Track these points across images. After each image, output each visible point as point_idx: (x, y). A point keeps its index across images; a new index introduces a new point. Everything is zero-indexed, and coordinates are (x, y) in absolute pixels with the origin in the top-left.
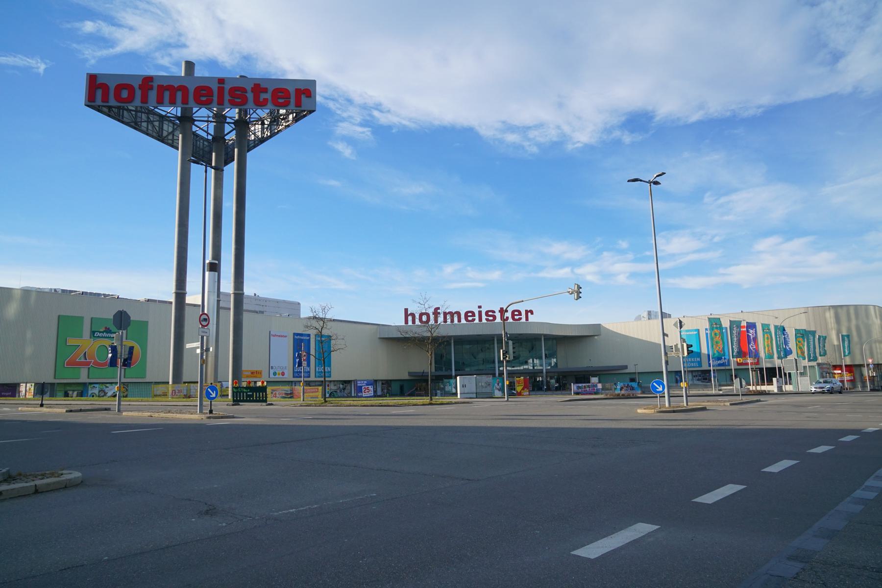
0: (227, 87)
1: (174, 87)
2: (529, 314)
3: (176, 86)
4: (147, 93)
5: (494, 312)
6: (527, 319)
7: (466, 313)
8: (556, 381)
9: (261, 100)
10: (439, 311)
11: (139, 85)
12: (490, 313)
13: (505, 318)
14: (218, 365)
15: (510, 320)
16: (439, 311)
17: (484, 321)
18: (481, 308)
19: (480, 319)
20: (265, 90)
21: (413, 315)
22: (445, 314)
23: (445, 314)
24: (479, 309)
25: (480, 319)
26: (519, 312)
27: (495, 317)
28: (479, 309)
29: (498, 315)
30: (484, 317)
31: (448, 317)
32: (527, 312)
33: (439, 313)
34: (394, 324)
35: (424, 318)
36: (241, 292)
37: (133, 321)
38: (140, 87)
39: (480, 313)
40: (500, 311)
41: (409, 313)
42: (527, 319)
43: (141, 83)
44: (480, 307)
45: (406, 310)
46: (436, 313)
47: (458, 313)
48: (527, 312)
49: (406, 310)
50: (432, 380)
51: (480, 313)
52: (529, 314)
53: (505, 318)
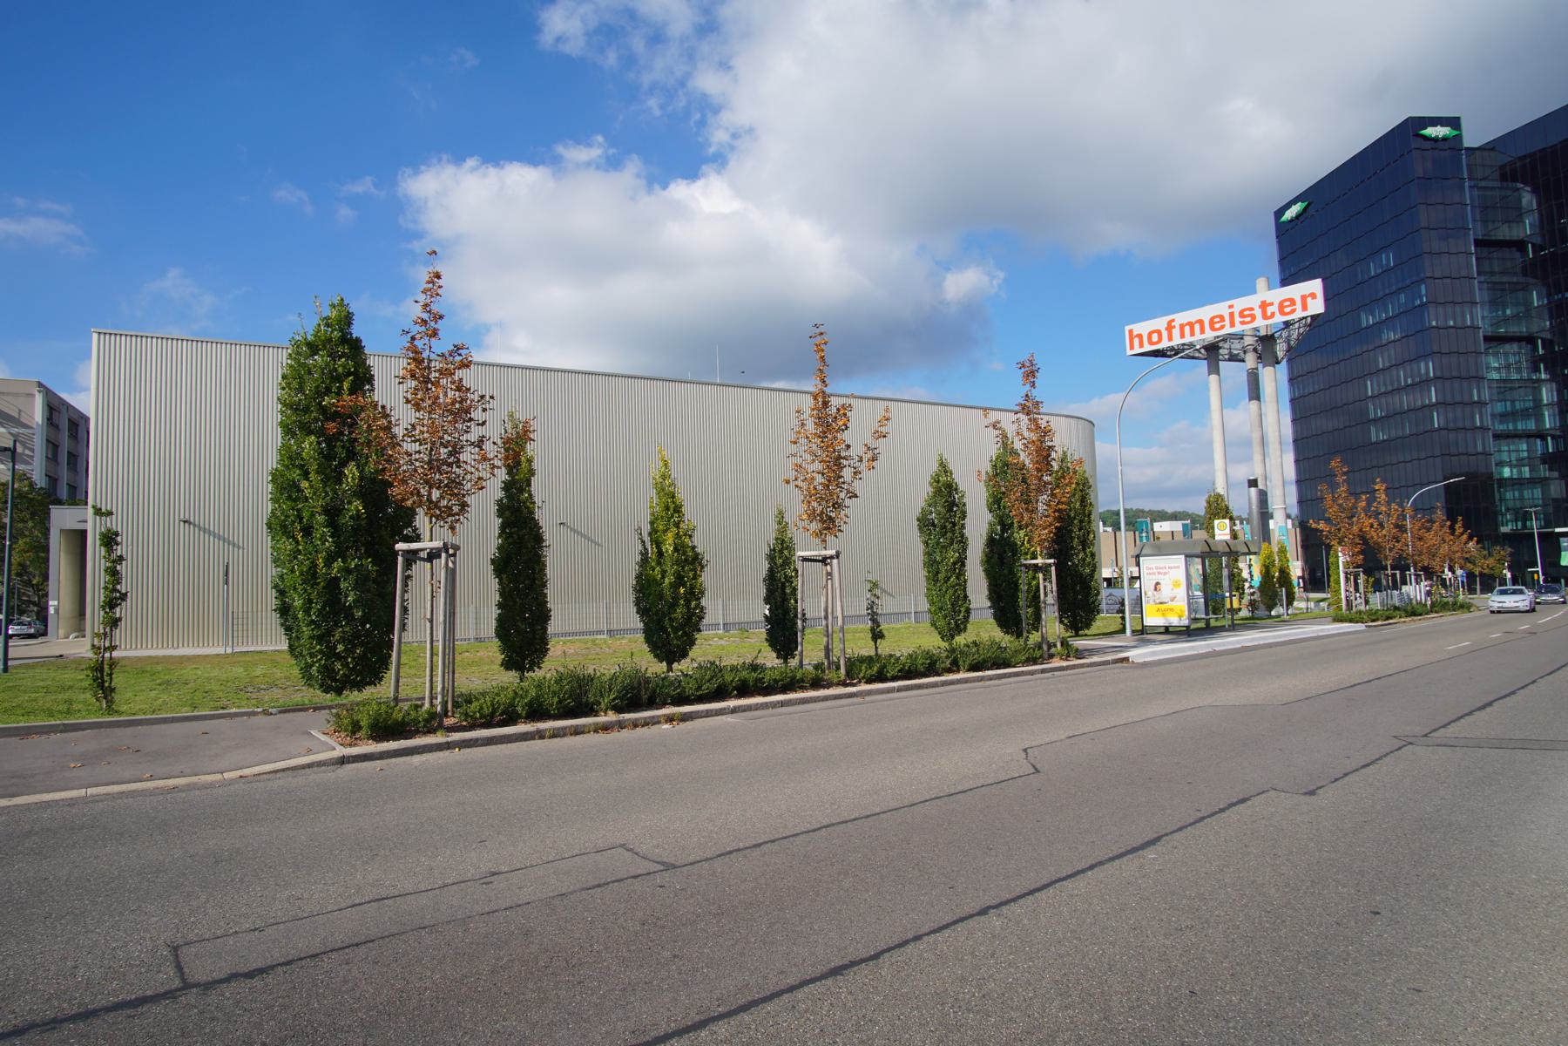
2: (1309, 299)
5: (1252, 309)
9: (1269, 314)
10: (1173, 324)
12: (1246, 313)
13: (1269, 314)
16: (1173, 324)
20: (1271, 304)
21: (1140, 336)
22: (1182, 327)
23: (1182, 327)
27: (1253, 318)
29: (1258, 312)
30: (1237, 319)
31: (1187, 329)
33: (1174, 327)
35: (1155, 338)
39: (1232, 315)
40: (1260, 307)
41: (1135, 333)
48: (1304, 298)
51: (1232, 315)
52: (1309, 299)
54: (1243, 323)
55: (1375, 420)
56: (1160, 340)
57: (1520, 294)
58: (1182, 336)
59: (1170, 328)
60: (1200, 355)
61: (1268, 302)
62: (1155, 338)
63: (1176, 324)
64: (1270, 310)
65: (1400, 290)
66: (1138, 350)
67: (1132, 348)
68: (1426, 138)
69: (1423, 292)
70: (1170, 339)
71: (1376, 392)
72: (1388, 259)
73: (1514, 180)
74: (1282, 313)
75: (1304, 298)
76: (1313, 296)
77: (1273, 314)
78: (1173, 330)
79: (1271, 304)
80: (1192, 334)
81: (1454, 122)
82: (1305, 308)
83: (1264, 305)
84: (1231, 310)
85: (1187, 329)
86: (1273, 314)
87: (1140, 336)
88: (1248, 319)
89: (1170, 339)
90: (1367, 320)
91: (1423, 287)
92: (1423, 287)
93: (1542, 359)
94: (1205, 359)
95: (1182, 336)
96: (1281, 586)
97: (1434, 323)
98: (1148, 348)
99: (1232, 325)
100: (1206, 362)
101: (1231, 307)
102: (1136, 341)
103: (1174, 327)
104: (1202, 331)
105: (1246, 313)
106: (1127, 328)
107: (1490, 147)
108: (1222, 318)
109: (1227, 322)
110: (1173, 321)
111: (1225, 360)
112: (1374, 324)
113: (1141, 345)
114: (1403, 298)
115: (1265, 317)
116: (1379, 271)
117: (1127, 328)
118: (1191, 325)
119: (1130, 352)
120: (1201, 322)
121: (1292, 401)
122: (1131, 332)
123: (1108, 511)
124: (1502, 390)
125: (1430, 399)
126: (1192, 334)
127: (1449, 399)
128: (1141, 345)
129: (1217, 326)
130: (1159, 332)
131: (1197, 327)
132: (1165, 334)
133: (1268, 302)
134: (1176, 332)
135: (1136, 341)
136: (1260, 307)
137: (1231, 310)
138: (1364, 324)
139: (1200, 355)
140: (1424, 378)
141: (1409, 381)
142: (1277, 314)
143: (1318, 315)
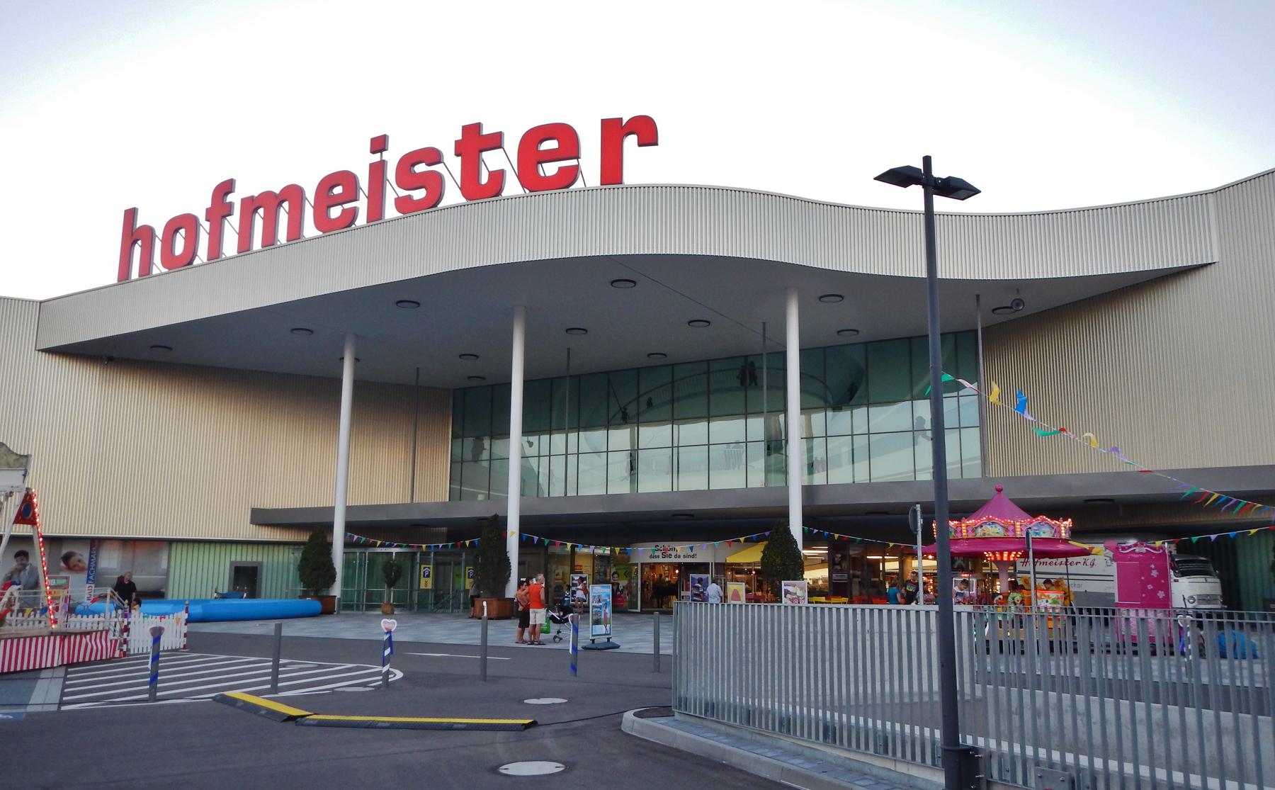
0: (392, 157)
1: (275, 193)
2: (631, 142)
3: (277, 191)
4: (1072, 752)
6: (612, 169)
8: (913, 559)
13: (484, 179)
15: (512, 187)
17: (391, 211)
19: (376, 212)
20: (495, 141)
21: (148, 232)
24: (376, 158)
25: (376, 212)
26: (567, 137)
27: (435, 185)
28: (376, 158)
29: (452, 167)
30: (392, 192)
32: (613, 132)
36: (348, 550)
37: (284, 636)
38: (210, 215)
39: (377, 171)
42: (612, 169)
43: (209, 205)
44: (379, 144)
45: (131, 215)
46: (219, 210)
48: (613, 132)
49: (131, 215)
52: (631, 142)
53: (484, 179)
61: (486, 131)
79: (495, 141)
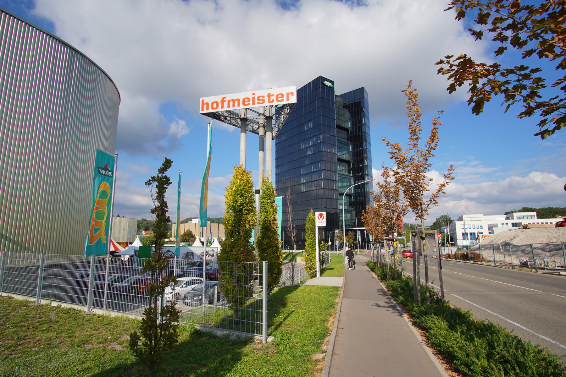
2: (290, 95)
5: (263, 97)
7: (244, 99)
9: (271, 100)
10: (225, 99)
11: (532, 49)
12: (260, 98)
13: (271, 100)
14: (207, 183)
16: (225, 99)
18: (481, 228)
20: (273, 95)
21: (207, 104)
22: (229, 101)
23: (229, 101)
27: (264, 101)
29: (266, 99)
30: (256, 101)
31: (231, 103)
34: (84, 41)
35: (215, 105)
39: (254, 98)
41: (205, 102)
43: (482, 37)
47: (238, 100)
48: (288, 94)
50: (345, 195)
51: (254, 98)
52: (290, 95)
54: (258, 103)
55: (303, 184)
56: (217, 107)
57: (347, 146)
58: (229, 106)
59: (223, 101)
60: (238, 125)
61: (271, 94)
62: (215, 105)
63: (226, 100)
64: (272, 98)
65: (314, 136)
66: (205, 111)
67: (203, 110)
68: (324, 84)
69: (321, 138)
70: (222, 107)
71: (308, 163)
72: (311, 125)
73: (347, 108)
74: (278, 101)
75: (288, 94)
76: (292, 94)
77: (273, 101)
78: (224, 103)
79: (273, 95)
80: (234, 106)
81: (332, 82)
82: (288, 99)
83: (269, 96)
84: (254, 96)
85: (231, 103)
86: (273, 101)
87: (207, 104)
88: (261, 102)
89: (222, 107)
90: (302, 146)
91: (321, 136)
92: (321, 136)
93: (352, 169)
94: (240, 128)
95: (229, 106)
96: (262, 260)
97: (324, 150)
98: (211, 111)
99: (254, 104)
100: (240, 129)
101: (254, 94)
102: (205, 106)
103: (225, 101)
104: (239, 105)
105: (260, 98)
106: (201, 99)
107: (341, 96)
108: (249, 99)
109: (251, 102)
110: (225, 98)
111: (250, 131)
112: (305, 148)
113: (207, 109)
114: (314, 139)
115: (269, 102)
116: (307, 129)
117: (201, 99)
118: (234, 101)
119: (201, 112)
120: (238, 100)
121: (276, 174)
122: (203, 101)
123: (215, 218)
124: (341, 178)
125: (321, 177)
126: (234, 106)
127: (327, 178)
128: (207, 109)
129: (246, 103)
130: (217, 103)
131: (236, 102)
132: (220, 104)
133: (271, 94)
134: (226, 104)
135: (205, 106)
136: (267, 96)
137: (254, 96)
138: (302, 148)
139: (238, 125)
140: (320, 169)
141: (315, 170)
142: (275, 100)
143: (295, 103)
